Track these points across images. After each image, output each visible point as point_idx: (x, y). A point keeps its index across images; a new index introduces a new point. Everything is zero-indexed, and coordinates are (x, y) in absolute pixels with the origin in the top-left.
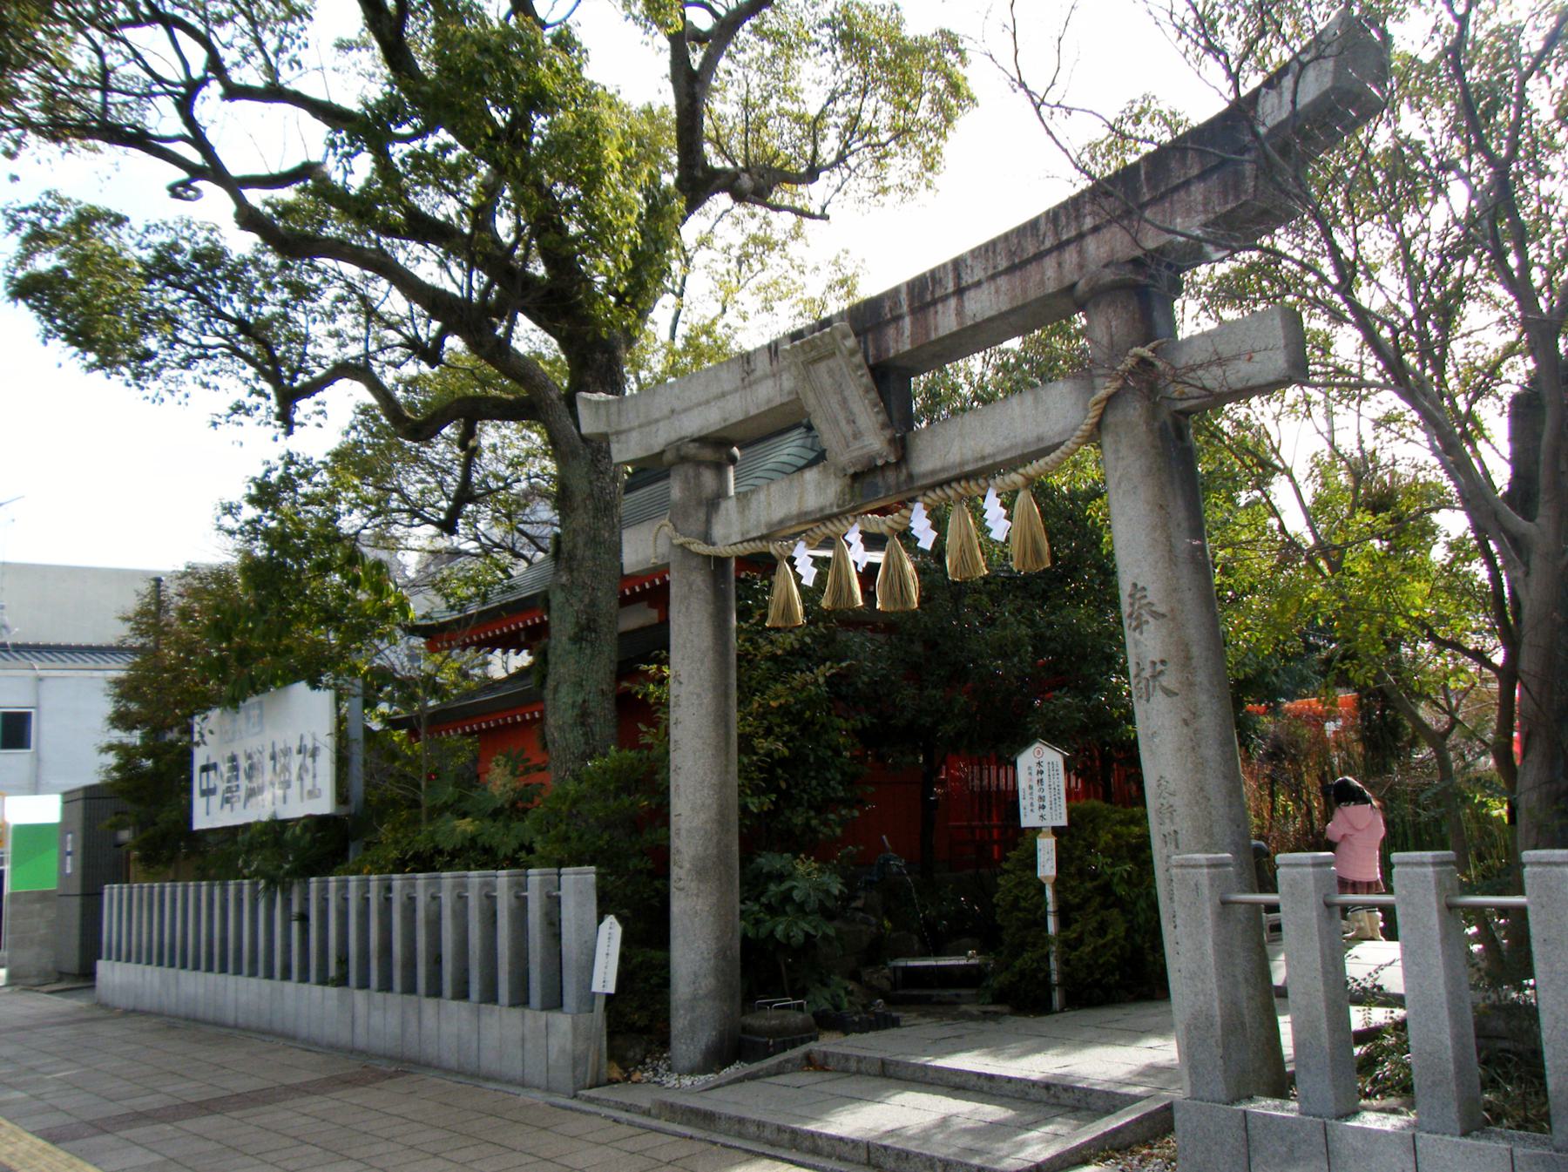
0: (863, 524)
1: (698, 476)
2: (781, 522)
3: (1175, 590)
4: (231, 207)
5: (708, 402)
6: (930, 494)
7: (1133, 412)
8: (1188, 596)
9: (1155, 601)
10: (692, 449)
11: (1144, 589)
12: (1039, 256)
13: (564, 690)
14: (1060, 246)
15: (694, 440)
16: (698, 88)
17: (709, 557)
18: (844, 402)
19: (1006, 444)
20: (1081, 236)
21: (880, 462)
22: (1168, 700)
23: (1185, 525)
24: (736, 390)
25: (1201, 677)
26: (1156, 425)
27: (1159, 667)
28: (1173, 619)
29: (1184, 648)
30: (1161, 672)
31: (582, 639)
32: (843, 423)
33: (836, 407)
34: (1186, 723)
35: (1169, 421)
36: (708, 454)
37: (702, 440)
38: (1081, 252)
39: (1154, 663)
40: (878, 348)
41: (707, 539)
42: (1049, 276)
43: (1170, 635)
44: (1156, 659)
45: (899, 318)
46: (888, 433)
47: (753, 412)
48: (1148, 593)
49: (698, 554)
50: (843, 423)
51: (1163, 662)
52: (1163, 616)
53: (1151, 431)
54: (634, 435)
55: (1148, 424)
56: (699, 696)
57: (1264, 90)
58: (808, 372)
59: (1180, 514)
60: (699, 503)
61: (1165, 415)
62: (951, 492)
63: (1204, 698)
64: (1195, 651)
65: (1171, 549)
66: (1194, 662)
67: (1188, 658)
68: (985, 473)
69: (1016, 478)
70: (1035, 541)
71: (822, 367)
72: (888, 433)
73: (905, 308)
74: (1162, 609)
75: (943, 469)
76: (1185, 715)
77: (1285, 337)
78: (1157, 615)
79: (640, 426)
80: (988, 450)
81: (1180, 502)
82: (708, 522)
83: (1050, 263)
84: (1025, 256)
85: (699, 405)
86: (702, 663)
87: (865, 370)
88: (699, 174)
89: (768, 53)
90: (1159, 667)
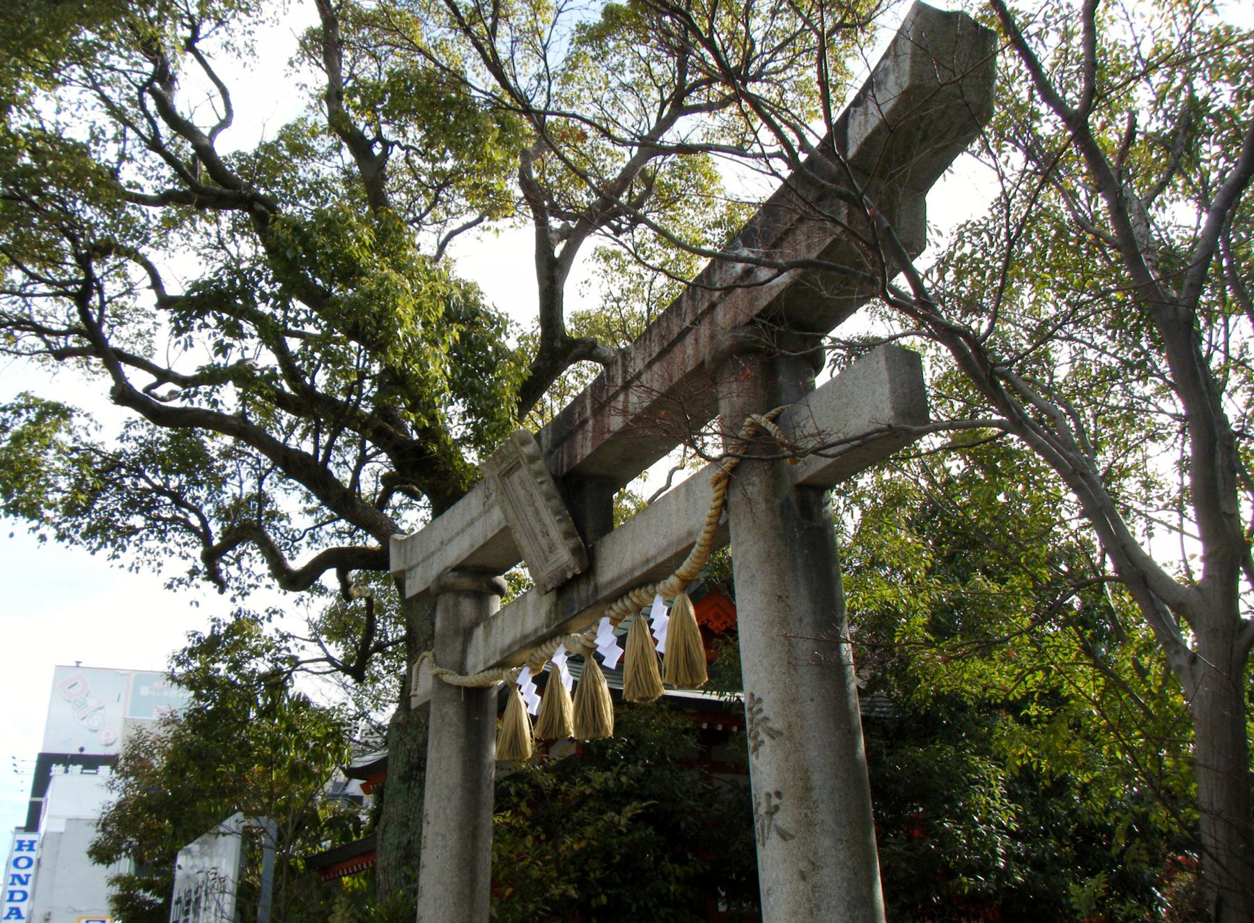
0: (566, 646)
1: (457, 605)
2: (510, 647)
3: (793, 701)
4: (108, 382)
5: (463, 531)
6: (614, 607)
7: (755, 485)
8: (810, 707)
9: (771, 716)
10: (451, 578)
11: (760, 700)
12: (683, 334)
13: (392, 829)
14: (697, 321)
15: (454, 570)
16: (557, 273)
17: (459, 687)
18: (537, 512)
19: (665, 543)
20: (713, 306)
21: (569, 575)
22: (782, 844)
23: (808, 619)
24: (480, 516)
25: (824, 815)
26: (778, 501)
27: (775, 801)
28: (791, 738)
29: (803, 775)
30: (777, 808)
31: (411, 778)
32: (540, 536)
33: (531, 518)
34: (803, 876)
35: (793, 498)
36: (466, 583)
37: (460, 568)
38: (712, 323)
39: (768, 795)
40: (570, 457)
41: (462, 670)
42: (690, 353)
43: (787, 759)
44: (772, 792)
45: (584, 422)
46: (572, 543)
47: (490, 535)
48: (764, 706)
49: (450, 685)
50: (540, 536)
51: (778, 794)
52: (780, 733)
53: (771, 509)
54: (420, 569)
55: (767, 501)
56: (444, 837)
57: (852, 110)
58: (504, 484)
59: (802, 604)
60: (456, 633)
61: (787, 491)
62: (627, 602)
63: (826, 842)
64: (817, 779)
65: (790, 650)
66: (815, 794)
67: (808, 789)
68: (650, 579)
69: (673, 580)
70: (687, 650)
71: (515, 478)
72: (572, 543)
73: (589, 412)
74: (777, 725)
75: (619, 578)
76: (803, 865)
77: (891, 381)
78: (773, 734)
79: (423, 561)
80: (652, 552)
81: (803, 590)
82: (464, 652)
83: (689, 340)
84: (672, 338)
85: (458, 534)
86: (449, 799)
87: (547, 477)
88: (558, 344)
89: (673, 257)
90: (775, 801)
